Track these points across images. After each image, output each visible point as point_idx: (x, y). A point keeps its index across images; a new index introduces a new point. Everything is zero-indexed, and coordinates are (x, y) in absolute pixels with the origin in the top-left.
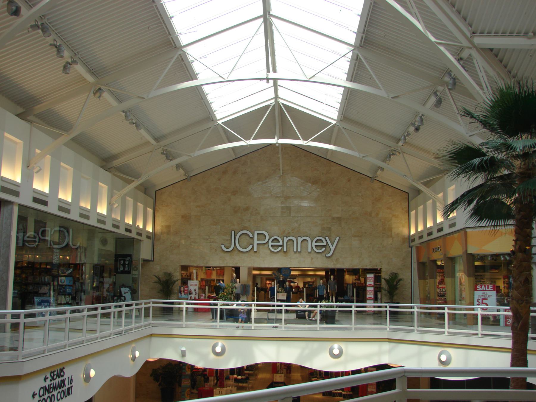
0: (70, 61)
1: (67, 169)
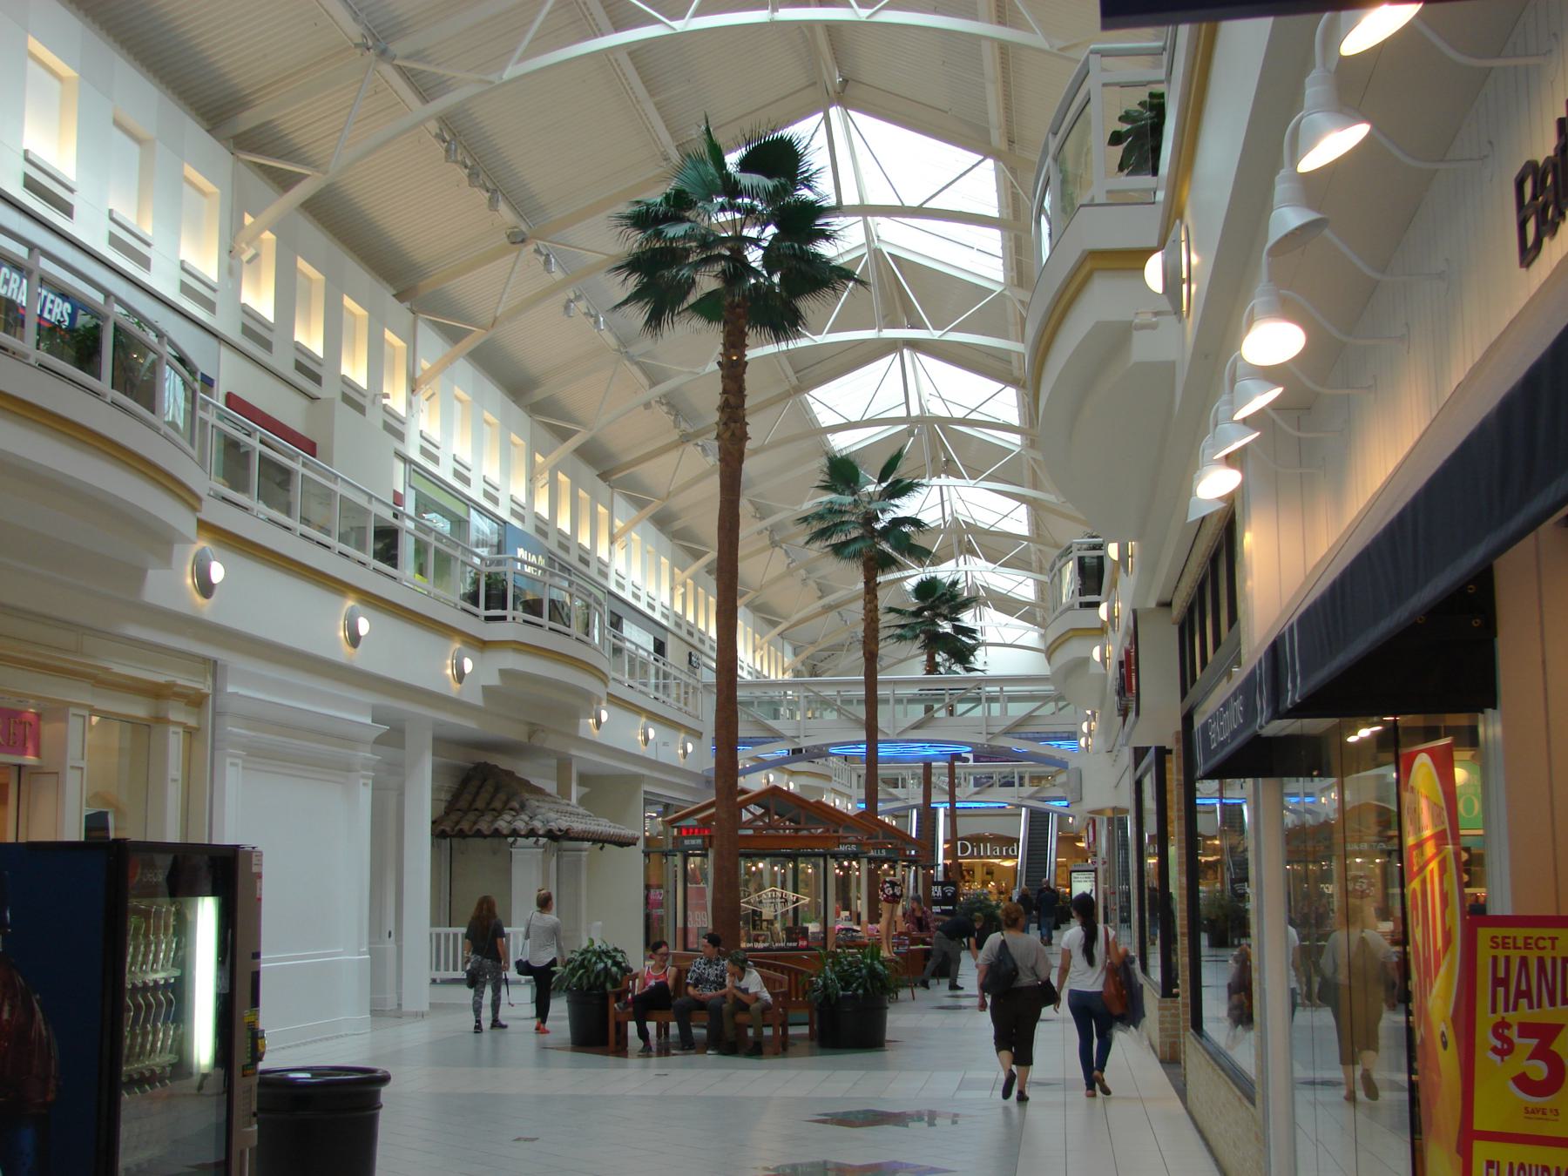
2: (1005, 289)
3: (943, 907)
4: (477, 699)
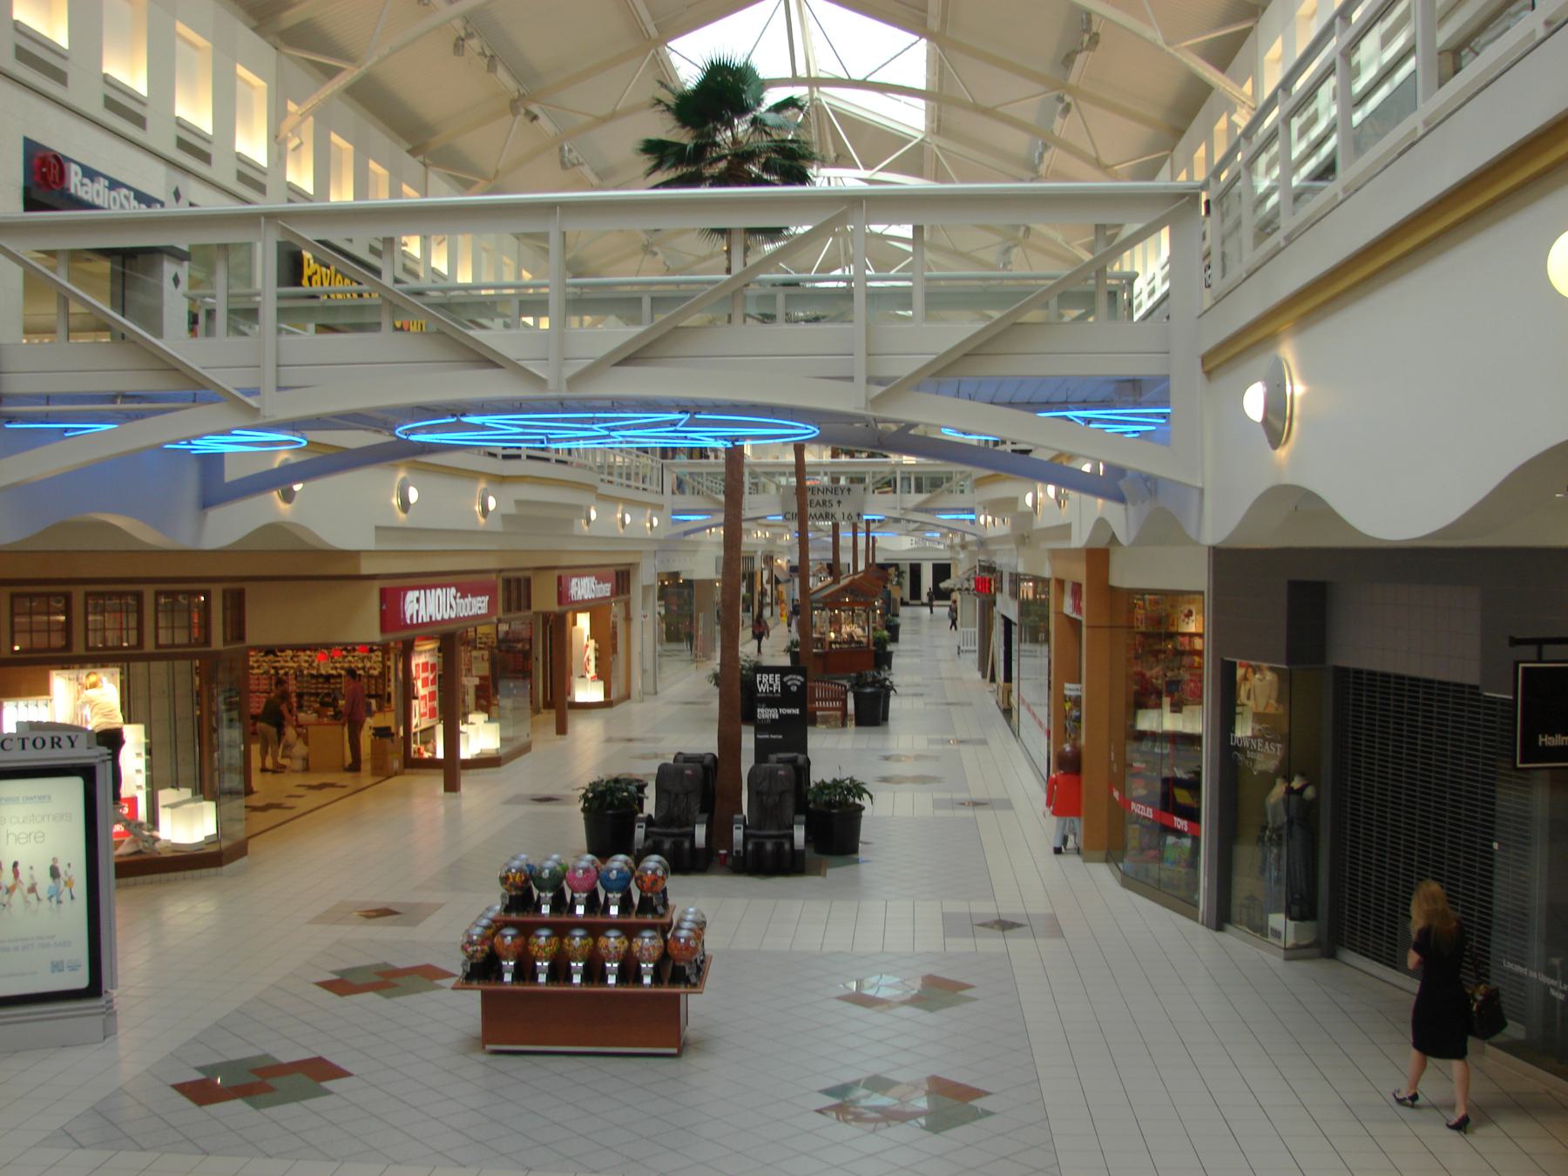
0: (463, 34)
1: (253, 85)
2: (926, 136)
3: (783, 711)
4: (498, 526)
